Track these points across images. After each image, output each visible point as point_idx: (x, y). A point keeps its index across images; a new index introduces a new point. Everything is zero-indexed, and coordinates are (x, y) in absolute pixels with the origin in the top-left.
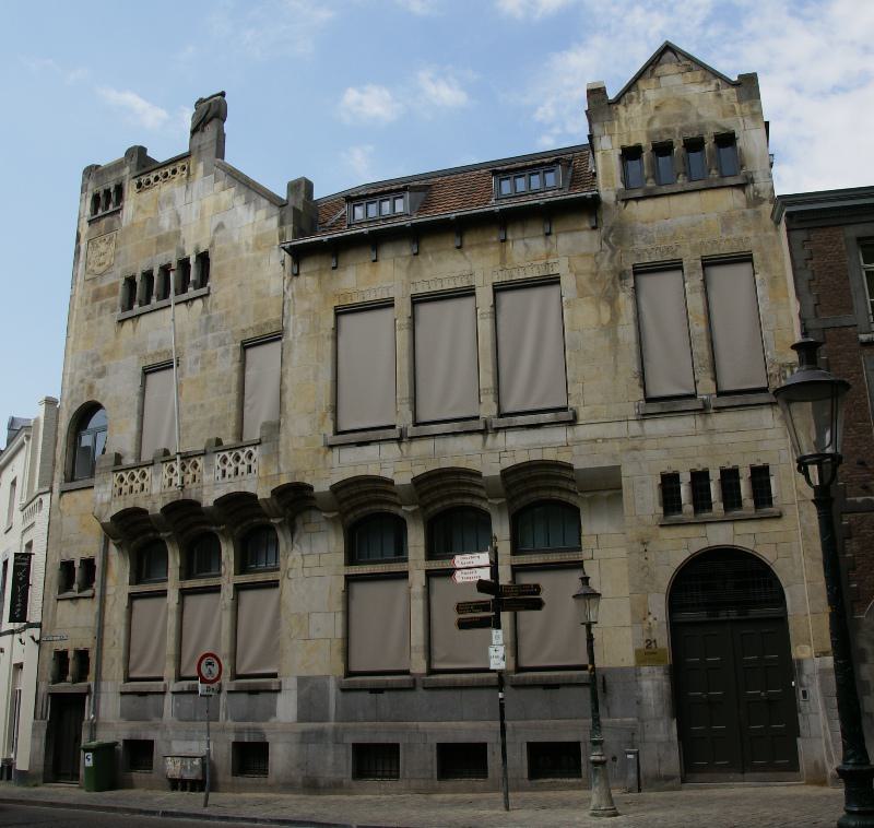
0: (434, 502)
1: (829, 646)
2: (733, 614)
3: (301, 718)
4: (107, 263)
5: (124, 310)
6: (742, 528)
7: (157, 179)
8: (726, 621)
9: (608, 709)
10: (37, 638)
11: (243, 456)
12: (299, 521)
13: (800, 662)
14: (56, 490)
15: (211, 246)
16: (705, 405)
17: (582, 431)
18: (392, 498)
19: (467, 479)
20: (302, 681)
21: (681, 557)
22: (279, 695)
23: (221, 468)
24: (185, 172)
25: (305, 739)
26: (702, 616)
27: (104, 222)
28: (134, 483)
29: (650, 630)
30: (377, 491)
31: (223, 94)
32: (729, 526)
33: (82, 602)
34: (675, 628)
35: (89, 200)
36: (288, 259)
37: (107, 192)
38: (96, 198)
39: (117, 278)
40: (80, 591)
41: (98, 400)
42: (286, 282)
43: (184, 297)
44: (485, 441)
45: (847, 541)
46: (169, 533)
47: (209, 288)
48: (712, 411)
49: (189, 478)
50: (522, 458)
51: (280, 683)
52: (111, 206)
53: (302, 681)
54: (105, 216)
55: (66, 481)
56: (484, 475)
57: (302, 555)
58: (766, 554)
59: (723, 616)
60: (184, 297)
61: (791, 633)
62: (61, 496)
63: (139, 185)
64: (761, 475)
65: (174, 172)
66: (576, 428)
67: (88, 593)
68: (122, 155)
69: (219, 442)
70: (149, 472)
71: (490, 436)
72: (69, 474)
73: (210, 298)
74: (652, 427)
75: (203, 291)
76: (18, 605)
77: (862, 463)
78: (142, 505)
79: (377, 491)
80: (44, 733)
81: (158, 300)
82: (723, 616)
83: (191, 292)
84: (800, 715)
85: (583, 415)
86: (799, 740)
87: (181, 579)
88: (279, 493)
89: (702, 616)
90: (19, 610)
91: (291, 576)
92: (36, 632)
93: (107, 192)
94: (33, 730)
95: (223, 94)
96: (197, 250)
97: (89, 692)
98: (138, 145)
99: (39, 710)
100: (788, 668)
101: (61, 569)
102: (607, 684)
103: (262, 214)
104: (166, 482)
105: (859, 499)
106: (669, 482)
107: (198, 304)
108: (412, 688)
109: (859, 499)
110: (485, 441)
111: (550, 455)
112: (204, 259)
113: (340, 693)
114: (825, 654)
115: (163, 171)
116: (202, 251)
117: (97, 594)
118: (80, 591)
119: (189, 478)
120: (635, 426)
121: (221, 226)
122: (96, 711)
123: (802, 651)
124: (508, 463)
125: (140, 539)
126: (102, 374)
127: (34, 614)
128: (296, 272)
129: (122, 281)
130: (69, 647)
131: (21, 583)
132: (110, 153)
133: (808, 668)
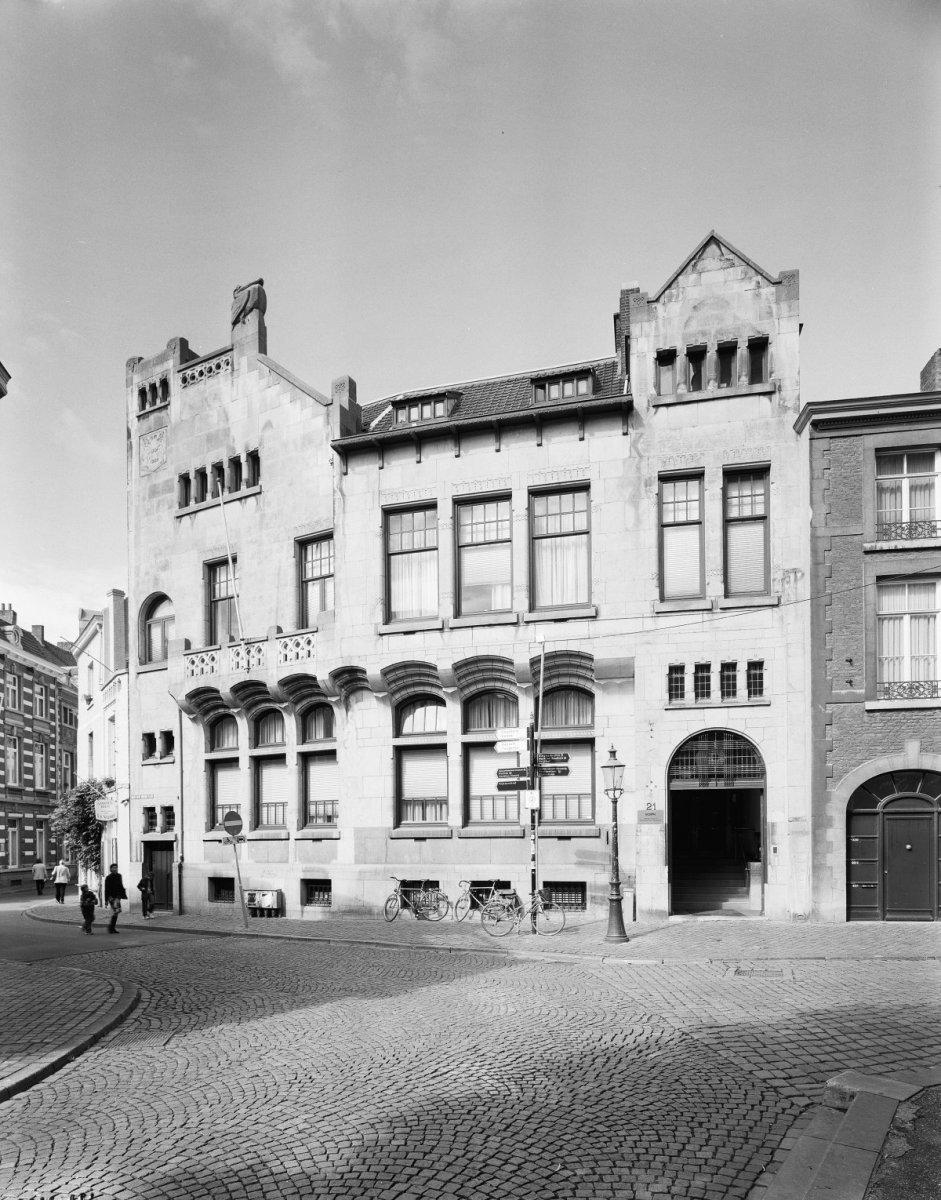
4: (160, 460)
18: (589, 674)
20: (358, 831)
27: (152, 417)
40: (161, 758)
41: (165, 591)
43: (238, 495)
52: (158, 401)
53: (358, 831)
58: (754, 736)
60: (238, 495)
62: (137, 677)
63: (184, 380)
65: (218, 366)
70: (264, 646)
75: (255, 489)
83: (244, 490)
85: (603, 614)
103: (308, 412)
106: (676, 670)
111: (573, 647)
115: (208, 366)
118: (161, 758)
121: (268, 425)
129: (177, 479)
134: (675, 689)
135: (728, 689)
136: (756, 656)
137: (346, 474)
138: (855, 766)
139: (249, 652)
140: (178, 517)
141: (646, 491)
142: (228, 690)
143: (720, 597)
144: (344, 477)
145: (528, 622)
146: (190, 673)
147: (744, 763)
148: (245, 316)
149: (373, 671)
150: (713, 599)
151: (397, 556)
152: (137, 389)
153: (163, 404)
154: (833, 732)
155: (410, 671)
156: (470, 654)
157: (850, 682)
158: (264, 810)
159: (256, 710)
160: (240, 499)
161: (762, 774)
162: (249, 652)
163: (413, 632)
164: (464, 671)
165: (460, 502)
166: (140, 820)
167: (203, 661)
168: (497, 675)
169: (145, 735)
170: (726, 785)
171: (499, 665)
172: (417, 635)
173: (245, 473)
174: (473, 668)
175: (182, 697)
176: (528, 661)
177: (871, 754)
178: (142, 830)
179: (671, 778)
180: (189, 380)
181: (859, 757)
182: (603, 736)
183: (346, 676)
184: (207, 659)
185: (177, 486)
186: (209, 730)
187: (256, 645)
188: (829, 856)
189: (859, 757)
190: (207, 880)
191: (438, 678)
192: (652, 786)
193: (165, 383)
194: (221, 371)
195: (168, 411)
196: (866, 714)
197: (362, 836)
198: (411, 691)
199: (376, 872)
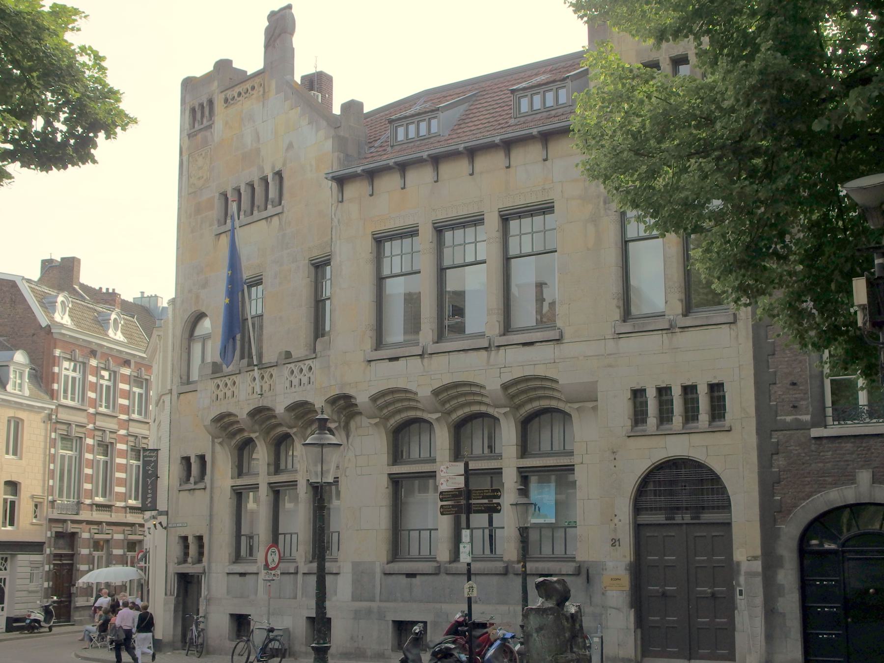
0: (455, 409)
1: (758, 552)
2: (687, 518)
3: (355, 598)
4: (205, 178)
5: (219, 225)
6: (696, 439)
7: (240, 94)
8: (681, 524)
9: (591, 597)
10: (165, 525)
11: (305, 369)
12: (352, 425)
13: (738, 564)
14: (175, 393)
15: (284, 164)
16: (671, 325)
17: (567, 349)
18: (556, 394)
19: (548, 384)
20: (356, 565)
21: (642, 466)
22: (338, 576)
23: (252, 386)
24: (261, 89)
25: (357, 615)
26: (660, 518)
27: (199, 136)
28: (292, 378)
29: (615, 530)
30: (544, 388)
31: (289, 7)
32: (686, 437)
33: (197, 492)
34: (638, 528)
35: (187, 112)
36: (335, 185)
37: (202, 106)
38: (193, 111)
39: (212, 194)
40: (195, 483)
41: (203, 310)
42: (333, 208)
43: (265, 214)
44: (489, 357)
45: (775, 457)
46: (257, 434)
47: (283, 207)
48: (677, 330)
49: (266, 387)
50: (518, 374)
51: (339, 567)
52: (205, 120)
53: (356, 565)
54: (201, 130)
55: (182, 384)
56: (560, 383)
57: (356, 456)
58: (716, 465)
59: (678, 519)
60: (265, 214)
61: (734, 537)
62: (178, 397)
63: (226, 101)
64: (716, 389)
65: (253, 88)
66: (562, 346)
67: (201, 485)
68: (210, 68)
69: (288, 355)
70: (274, 371)
71: (493, 353)
72: (185, 377)
73: (285, 215)
74: (627, 344)
75: (278, 209)
76: (150, 496)
77: (794, 384)
78: (232, 410)
79: (544, 388)
80: (172, 607)
81: (274, 206)
82: (678, 519)
83: (271, 210)
84: (736, 612)
85: (567, 337)
86: (736, 633)
87: (269, 474)
88: (333, 401)
89: (660, 518)
90: (149, 500)
91: (347, 474)
92: (163, 519)
93: (202, 106)
94: (165, 605)
95: (289, 7)
96: (273, 168)
97: (204, 572)
98: (54, 173)
99: (169, 588)
100: (730, 569)
101: (181, 463)
102: (590, 575)
103: (322, 133)
104: (250, 391)
105: (789, 419)
106: (638, 394)
107: (275, 220)
108: (436, 573)
109: (789, 419)
110: (489, 357)
111: (540, 371)
112: (279, 175)
113: (383, 575)
114: (755, 558)
115: (245, 87)
116: (277, 169)
117: (208, 486)
118: (195, 483)
119: (266, 387)
120: (611, 343)
121: (290, 146)
122: (209, 590)
123: (740, 555)
124: (507, 378)
125: (238, 437)
126: (205, 285)
127: (162, 505)
128: (340, 200)
129: (217, 195)
130: (190, 533)
131: (150, 476)
132: (202, 67)
133: (744, 568)
134: (639, 416)
135: (691, 414)
136: (715, 377)
137: (342, 201)
138: (804, 499)
139: (263, 377)
140: (217, 235)
141: (605, 209)
142: (245, 416)
143: (678, 315)
144: (340, 204)
145: (499, 346)
146: (214, 398)
147: (708, 494)
148: (275, 41)
149: (362, 398)
150: (672, 317)
151: (463, 235)
152: (189, 108)
153: (208, 124)
154: (780, 462)
155: (397, 396)
156: (447, 380)
157: (794, 407)
158: (281, 537)
159: (393, 422)
160: (266, 218)
161: (729, 507)
162: (263, 377)
163: (396, 359)
164: (444, 396)
165: (439, 230)
166: (177, 550)
167: (226, 385)
168: (540, 393)
169: (183, 458)
170: (667, 519)
171: (466, 389)
172: (402, 362)
173: (273, 193)
174: (453, 392)
175: (208, 422)
176: (499, 387)
177: (823, 486)
178: (176, 561)
179: (637, 509)
180: (229, 100)
181: (807, 489)
182: (582, 463)
183: (342, 402)
184: (229, 383)
185: (218, 204)
186: (520, 428)
187: (269, 370)
188: (781, 600)
189: (807, 489)
190: (228, 616)
191: (417, 401)
192: (616, 520)
193: (211, 102)
194: (254, 92)
195: (212, 130)
196: (813, 441)
197: (360, 572)
198: (467, 410)
199: (369, 611)
